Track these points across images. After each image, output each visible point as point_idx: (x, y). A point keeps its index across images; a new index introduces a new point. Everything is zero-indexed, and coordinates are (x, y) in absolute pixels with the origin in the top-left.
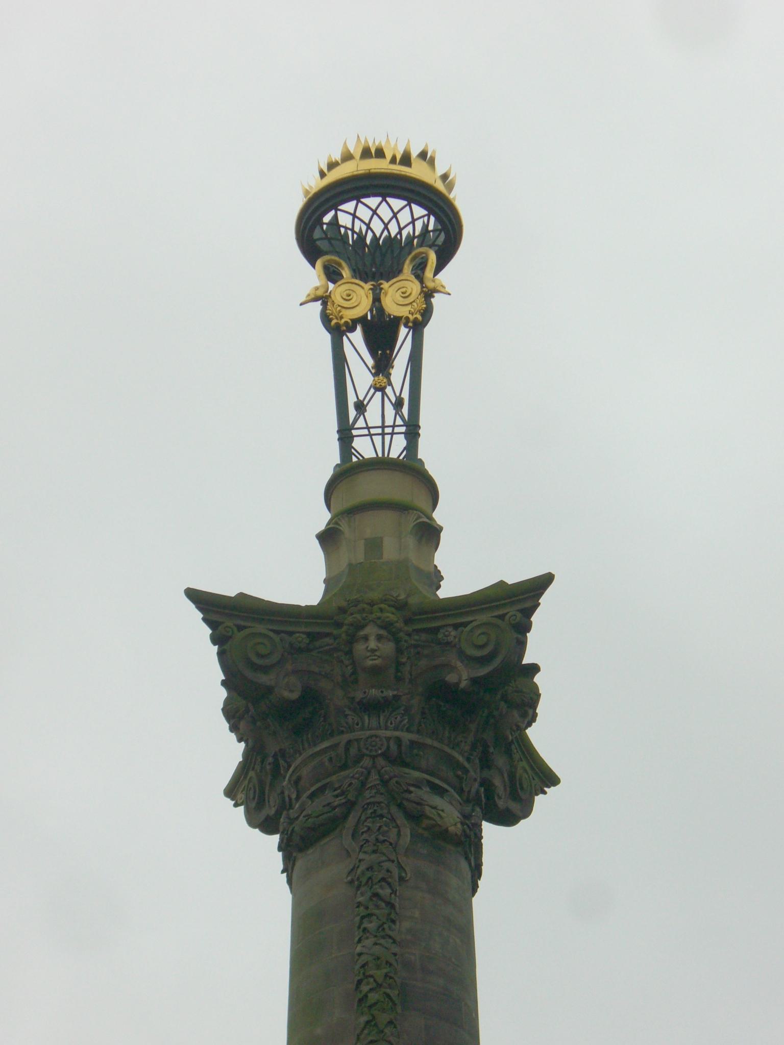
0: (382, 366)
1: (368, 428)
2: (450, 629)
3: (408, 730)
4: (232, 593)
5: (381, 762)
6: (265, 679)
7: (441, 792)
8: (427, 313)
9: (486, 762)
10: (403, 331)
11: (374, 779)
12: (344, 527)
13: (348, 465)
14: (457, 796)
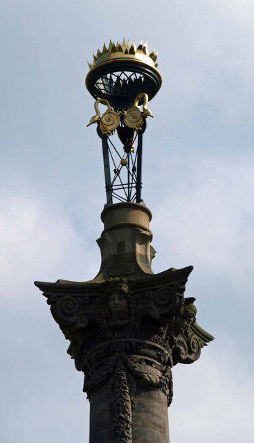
0: (128, 148)
1: (122, 185)
2: (151, 291)
3: (135, 337)
4: (53, 281)
5: (123, 353)
6: (72, 319)
7: (150, 363)
8: (144, 126)
9: (172, 343)
10: (135, 132)
11: (120, 362)
12: (108, 238)
13: (109, 205)
14: (158, 363)
